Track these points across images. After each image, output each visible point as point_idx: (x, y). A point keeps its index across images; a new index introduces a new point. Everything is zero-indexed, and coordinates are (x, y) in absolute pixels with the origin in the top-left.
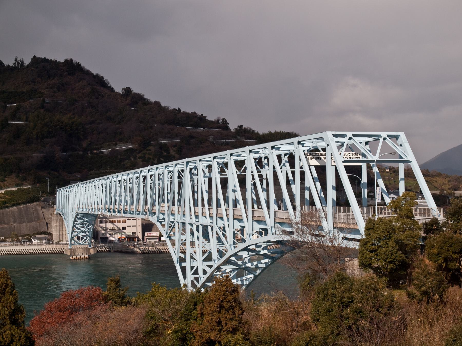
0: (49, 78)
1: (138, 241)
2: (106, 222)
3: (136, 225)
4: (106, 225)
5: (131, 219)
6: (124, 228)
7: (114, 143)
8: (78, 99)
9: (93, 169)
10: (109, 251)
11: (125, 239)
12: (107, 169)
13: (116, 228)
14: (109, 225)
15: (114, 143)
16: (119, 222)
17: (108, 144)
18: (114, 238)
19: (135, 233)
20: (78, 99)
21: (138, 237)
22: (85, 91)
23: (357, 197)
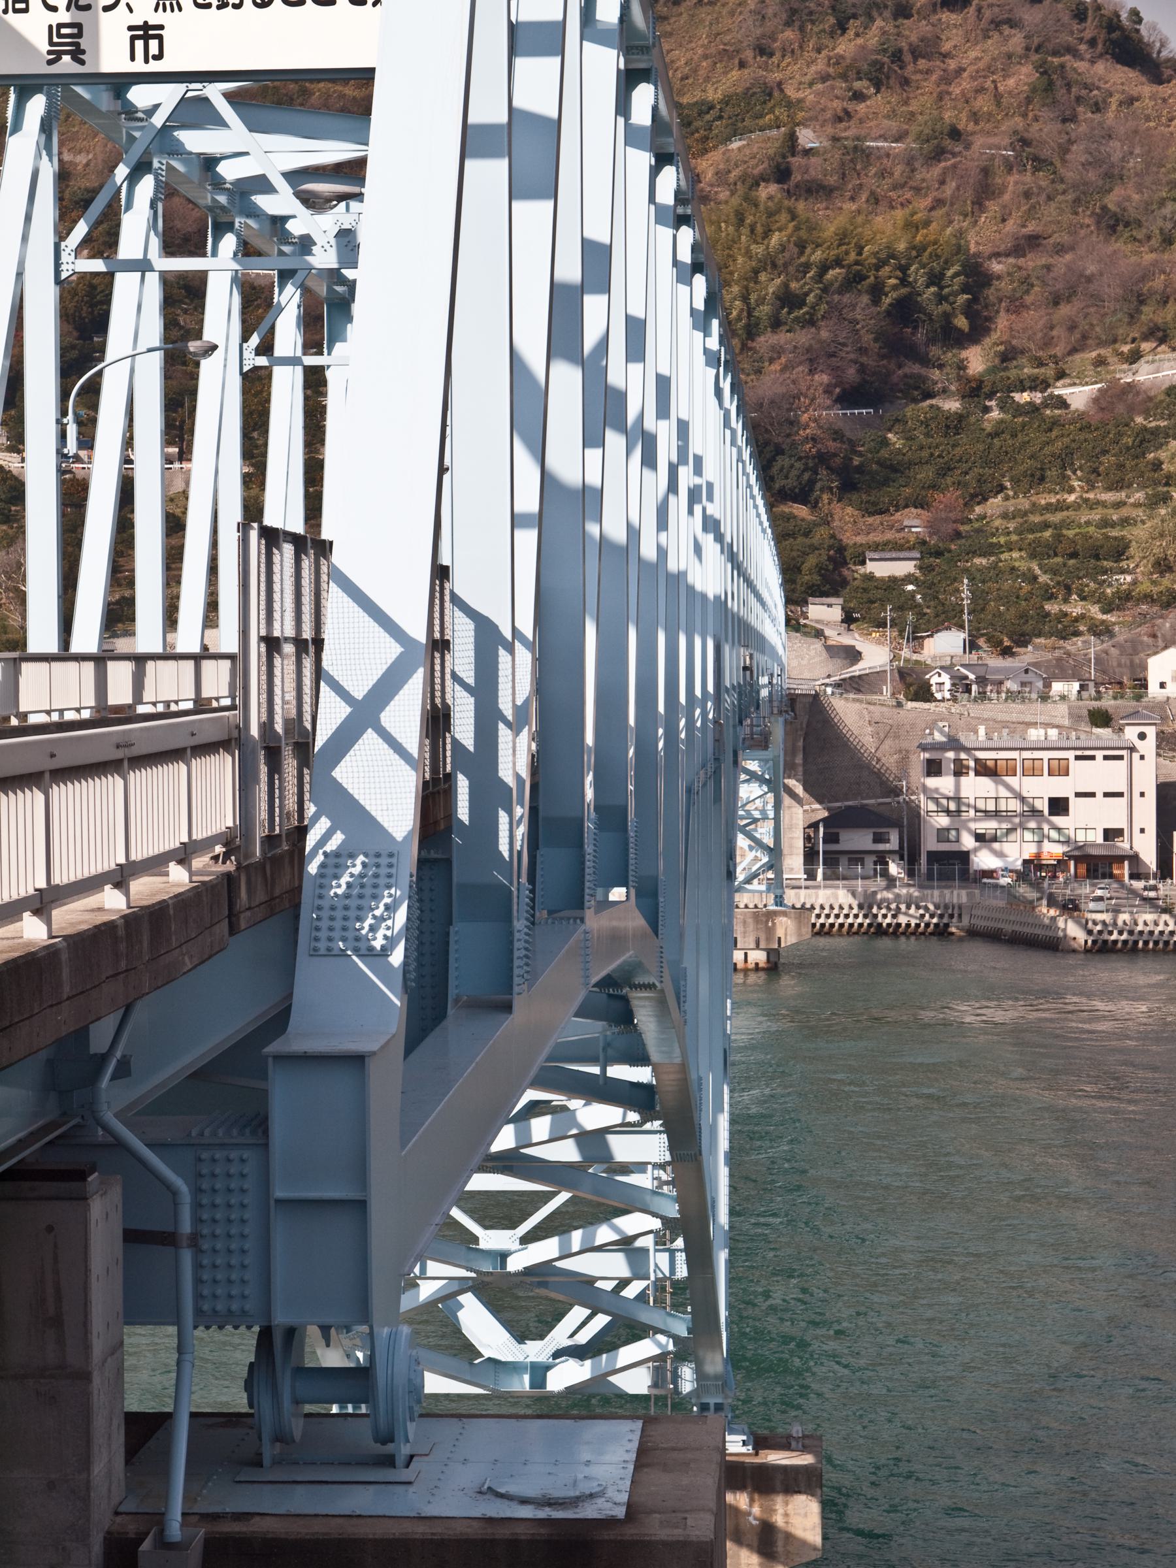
0: (844, 30)
1: (1134, 876)
2: (960, 771)
3: (1123, 788)
4: (957, 787)
5: (1099, 754)
6: (1059, 806)
7: (1126, 348)
8: (971, 127)
9: (1001, 488)
10: (941, 932)
11: (1061, 864)
12: (1071, 490)
13: (1014, 805)
14: (975, 788)
15: (1126, 348)
16: (1032, 771)
17: (1094, 354)
18: (1000, 855)
19: (1119, 832)
20: (971, 127)
21: (1134, 859)
22: (1011, 82)
23: (130, 602)
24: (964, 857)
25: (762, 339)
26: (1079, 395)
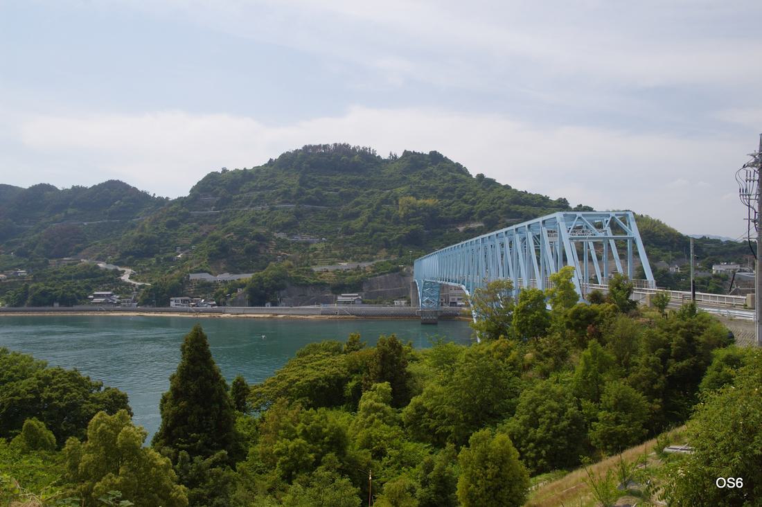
24: (456, 303)
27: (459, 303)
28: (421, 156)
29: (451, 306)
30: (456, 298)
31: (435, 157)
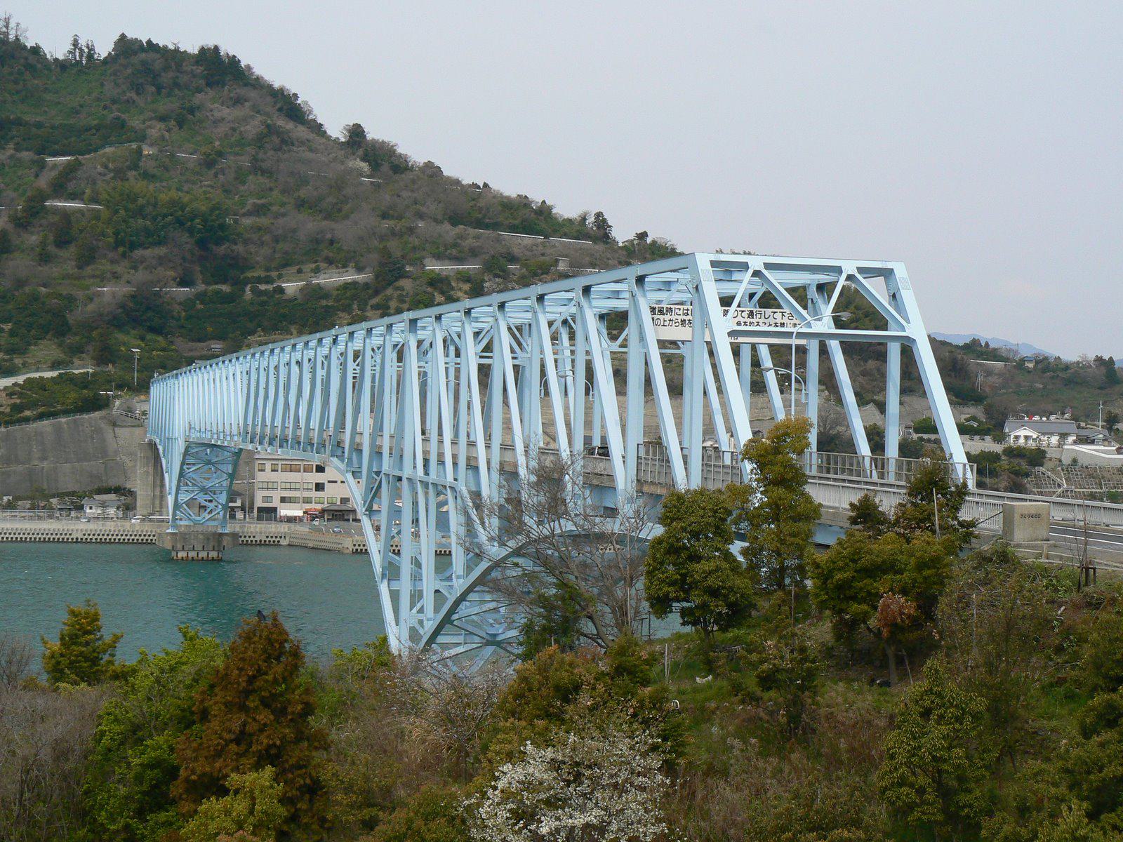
24: (275, 510)
25: (136, 251)
26: (292, 287)
27: (285, 511)
28: (174, 57)
29: (259, 518)
30: (276, 496)
31: (218, 69)
